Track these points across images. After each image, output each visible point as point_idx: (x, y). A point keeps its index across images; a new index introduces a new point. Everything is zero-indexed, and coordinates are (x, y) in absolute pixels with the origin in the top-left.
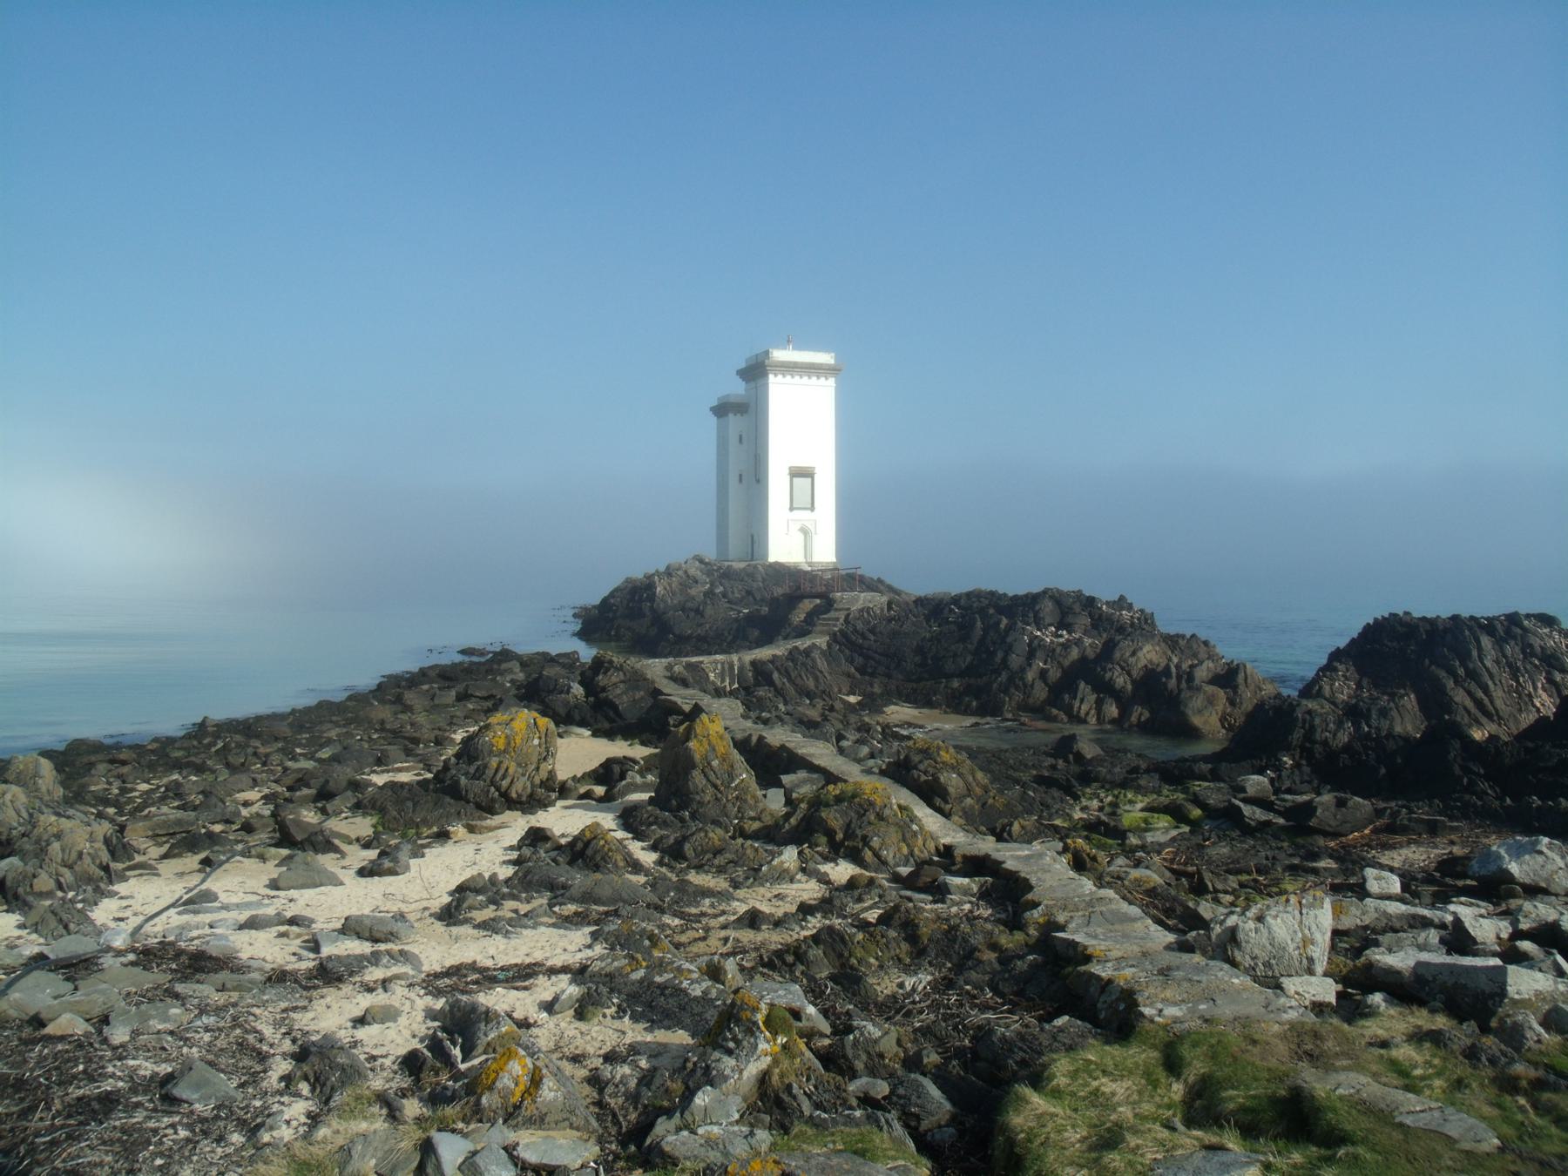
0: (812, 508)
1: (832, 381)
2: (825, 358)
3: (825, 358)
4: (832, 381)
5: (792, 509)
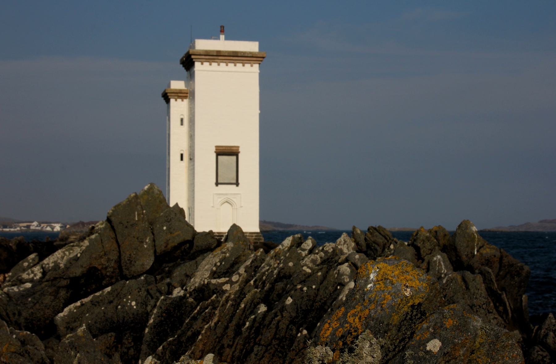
0: (237, 184)
1: (256, 67)
2: (252, 47)
3: (252, 47)
4: (256, 67)
5: (217, 184)
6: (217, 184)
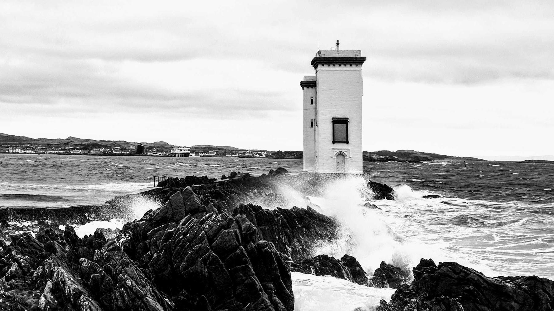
0: (347, 142)
5: (334, 142)
6: (334, 142)
